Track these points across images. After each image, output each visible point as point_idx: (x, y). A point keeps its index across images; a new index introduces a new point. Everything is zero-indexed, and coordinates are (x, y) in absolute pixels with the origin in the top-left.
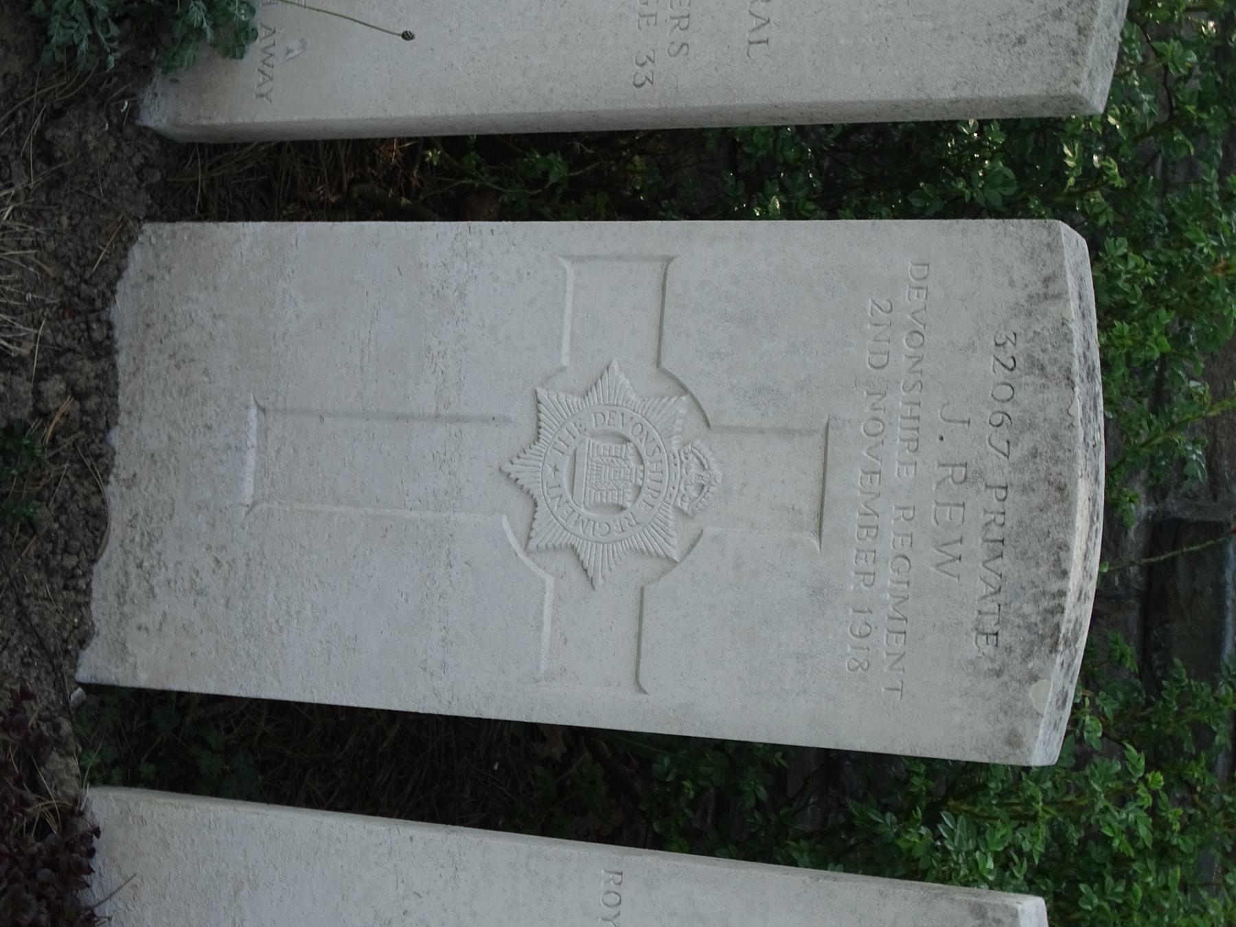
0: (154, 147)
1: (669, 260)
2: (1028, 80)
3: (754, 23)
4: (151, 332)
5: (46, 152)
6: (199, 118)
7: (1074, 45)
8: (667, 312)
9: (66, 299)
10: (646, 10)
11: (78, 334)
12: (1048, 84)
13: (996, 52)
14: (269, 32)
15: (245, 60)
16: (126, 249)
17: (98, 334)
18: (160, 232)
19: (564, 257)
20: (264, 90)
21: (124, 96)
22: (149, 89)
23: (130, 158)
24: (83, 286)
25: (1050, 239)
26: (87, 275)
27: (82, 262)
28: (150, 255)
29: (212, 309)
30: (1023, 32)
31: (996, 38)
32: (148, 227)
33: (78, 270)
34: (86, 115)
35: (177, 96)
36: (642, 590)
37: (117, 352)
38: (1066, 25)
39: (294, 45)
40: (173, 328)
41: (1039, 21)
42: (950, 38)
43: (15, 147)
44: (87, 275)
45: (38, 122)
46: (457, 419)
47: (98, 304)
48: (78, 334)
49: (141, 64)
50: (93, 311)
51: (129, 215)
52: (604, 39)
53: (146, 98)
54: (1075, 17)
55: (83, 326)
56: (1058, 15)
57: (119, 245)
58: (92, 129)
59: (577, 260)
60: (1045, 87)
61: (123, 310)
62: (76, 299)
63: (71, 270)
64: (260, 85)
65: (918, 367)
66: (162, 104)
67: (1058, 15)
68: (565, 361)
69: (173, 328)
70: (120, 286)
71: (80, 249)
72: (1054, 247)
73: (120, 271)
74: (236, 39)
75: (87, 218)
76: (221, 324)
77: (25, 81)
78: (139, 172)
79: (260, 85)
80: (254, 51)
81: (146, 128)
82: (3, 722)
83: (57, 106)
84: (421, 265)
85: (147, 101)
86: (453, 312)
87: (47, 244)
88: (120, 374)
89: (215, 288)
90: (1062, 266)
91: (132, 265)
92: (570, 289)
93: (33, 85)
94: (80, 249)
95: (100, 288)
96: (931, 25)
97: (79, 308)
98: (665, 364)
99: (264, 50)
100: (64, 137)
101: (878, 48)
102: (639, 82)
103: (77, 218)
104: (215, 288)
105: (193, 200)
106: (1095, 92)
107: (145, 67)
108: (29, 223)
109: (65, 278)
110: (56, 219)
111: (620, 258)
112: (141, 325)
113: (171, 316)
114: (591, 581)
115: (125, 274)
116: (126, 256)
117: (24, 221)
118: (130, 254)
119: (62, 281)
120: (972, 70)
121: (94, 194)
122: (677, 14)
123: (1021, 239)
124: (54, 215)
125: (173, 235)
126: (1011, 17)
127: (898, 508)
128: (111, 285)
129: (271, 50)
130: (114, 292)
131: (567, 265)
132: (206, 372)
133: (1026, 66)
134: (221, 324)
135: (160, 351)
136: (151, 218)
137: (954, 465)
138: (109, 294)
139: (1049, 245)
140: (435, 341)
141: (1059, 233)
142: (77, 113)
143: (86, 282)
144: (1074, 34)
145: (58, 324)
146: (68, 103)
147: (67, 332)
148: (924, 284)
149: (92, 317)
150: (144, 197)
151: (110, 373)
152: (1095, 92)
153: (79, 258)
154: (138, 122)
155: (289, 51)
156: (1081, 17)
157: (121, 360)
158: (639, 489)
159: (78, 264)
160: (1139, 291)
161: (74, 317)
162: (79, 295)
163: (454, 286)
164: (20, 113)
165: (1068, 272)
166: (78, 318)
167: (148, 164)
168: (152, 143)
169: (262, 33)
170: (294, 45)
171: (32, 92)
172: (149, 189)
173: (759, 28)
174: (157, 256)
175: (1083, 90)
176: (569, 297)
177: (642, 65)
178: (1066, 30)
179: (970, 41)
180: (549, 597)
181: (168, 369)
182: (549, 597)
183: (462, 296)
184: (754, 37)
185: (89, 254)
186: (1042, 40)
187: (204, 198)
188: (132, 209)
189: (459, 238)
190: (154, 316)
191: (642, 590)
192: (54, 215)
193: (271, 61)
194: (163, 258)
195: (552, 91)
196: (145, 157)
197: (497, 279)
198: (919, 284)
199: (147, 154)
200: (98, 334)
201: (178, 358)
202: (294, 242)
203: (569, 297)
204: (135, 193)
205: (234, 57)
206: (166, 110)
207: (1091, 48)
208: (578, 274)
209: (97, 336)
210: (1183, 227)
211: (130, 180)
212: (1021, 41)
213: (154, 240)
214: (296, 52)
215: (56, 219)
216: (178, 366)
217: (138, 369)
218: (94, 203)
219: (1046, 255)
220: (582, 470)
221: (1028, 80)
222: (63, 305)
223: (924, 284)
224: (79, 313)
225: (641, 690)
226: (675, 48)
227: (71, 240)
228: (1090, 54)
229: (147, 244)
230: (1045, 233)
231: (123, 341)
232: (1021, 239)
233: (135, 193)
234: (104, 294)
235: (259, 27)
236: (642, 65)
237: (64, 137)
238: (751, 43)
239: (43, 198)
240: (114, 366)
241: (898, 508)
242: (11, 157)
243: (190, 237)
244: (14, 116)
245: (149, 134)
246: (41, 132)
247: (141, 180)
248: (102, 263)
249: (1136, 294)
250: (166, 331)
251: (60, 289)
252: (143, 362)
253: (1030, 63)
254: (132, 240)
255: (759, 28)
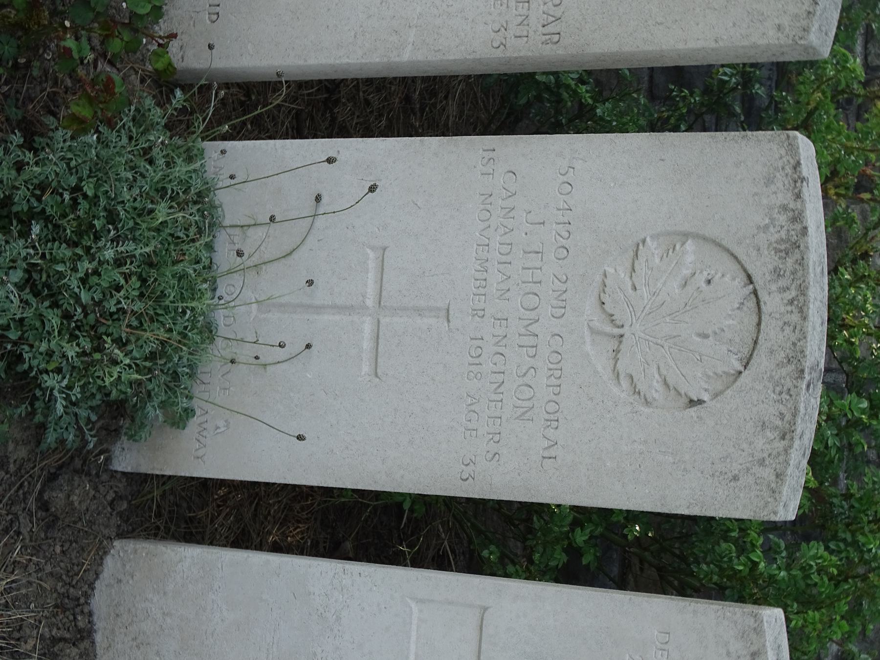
0: (121, 486)
1: (485, 609)
2: (741, 508)
3: (546, 444)
4: (119, 620)
5: (44, 506)
6: (153, 469)
7: (773, 485)
8: (484, 646)
9: (59, 601)
10: (470, 426)
11: (67, 625)
12: (755, 512)
13: (717, 484)
14: (203, 412)
15: (186, 431)
16: (102, 559)
17: (81, 622)
18: (126, 548)
19: (411, 599)
20: (200, 453)
21: (100, 453)
22: (118, 444)
23: (105, 496)
24: (72, 590)
25: (756, 625)
26: (74, 582)
27: (70, 574)
28: (119, 565)
29: (162, 608)
30: (736, 472)
31: (717, 474)
32: (117, 543)
33: (68, 580)
34: (73, 480)
35: (139, 452)
37: (95, 631)
38: (768, 470)
39: (221, 423)
40: (135, 619)
41: (748, 465)
42: (685, 470)
43: (23, 505)
44: (74, 582)
45: (39, 486)
47: (82, 600)
48: (67, 625)
49: (113, 428)
50: (79, 605)
51: (104, 536)
52: (440, 443)
53: (116, 450)
54: (774, 465)
55: (71, 618)
56: (762, 462)
57: (97, 557)
58: (77, 491)
60: (752, 514)
61: (101, 601)
62: (66, 601)
63: (63, 580)
64: (197, 450)
66: (128, 456)
67: (762, 462)
69: (135, 619)
70: (97, 584)
71: (69, 565)
72: (793, 149)
73: (97, 575)
74: (180, 419)
75: (74, 544)
76: (169, 620)
77: (29, 460)
78: (111, 503)
79: (197, 450)
80: (193, 424)
81: (116, 472)
82: (38, 2)
83: (53, 471)
84: (310, 593)
85: (117, 453)
86: (332, 630)
87: (45, 567)
88: (98, 648)
89: (165, 593)
90: (764, 646)
91: (106, 570)
92: (415, 622)
93: (36, 460)
94: (69, 565)
95: (83, 589)
96: (671, 459)
97: (69, 606)
99: (200, 424)
100: (57, 497)
101: (634, 472)
102: (465, 477)
103: (67, 545)
104: (165, 593)
105: (150, 508)
106: (821, 40)
107: (115, 430)
108: (32, 556)
109: (58, 588)
110: (52, 549)
111: (451, 603)
112: (112, 614)
113: (133, 610)
115: (101, 576)
116: (101, 564)
117: (28, 554)
118: (104, 562)
119: (56, 590)
120: (701, 495)
121: (79, 525)
122: (492, 431)
123: (736, 622)
124: (50, 545)
125: (135, 551)
126: (728, 460)
128: (91, 586)
129: (205, 426)
130: (93, 589)
131: (413, 605)
132: (158, 653)
133: (739, 497)
134: (169, 620)
135: (126, 635)
136: (121, 536)
138: (90, 592)
139: (755, 629)
140: (319, 650)
141: (762, 621)
142: (66, 477)
143: (73, 587)
144: (773, 478)
145: (53, 619)
146: (60, 467)
147: (60, 625)
148: (666, 647)
149: (78, 610)
150: (115, 520)
151: (90, 649)
152: (821, 40)
153: (68, 571)
154: (111, 468)
155: (218, 428)
156: (778, 466)
157: (98, 637)
159: (67, 575)
160: (826, 579)
161: (65, 612)
162: (68, 597)
163: (333, 611)
164: (26, 483)
165: (769, 649)
166: (67, 613)
167: (119, 497)
168: (120, 481)
169: (198, 412)
170: (221, 423)
171: (35, 466)
172: (120, 514)
173: (550, 447)
174: (124, 565)
175: (814, 38)
176: (414, 627)
177: (467, 465)
178: (768, 474)
179: (699, 475)
181: (131, 648)
183: (338, 619)
184: (546, 454)
185: (76, 568)
186: (751, 480)
187: (158, 506)
188: (106, 532)
189: (336, 576)
190: (122, 608)
192: (50, 545)
193: (205, 433)
194: (128, 567)
195: (402, 477)
196: (115, 492)
197: (363, 609)
198: (663, 646)
199: (117, 490)
200: (81, 622)
201: (138, 641)
202: (220, 566)
203: (414, 627)
204: (109, 519)
205: (178, 427)
206: (128, 459)
207: (785, 489)
208: (421, 611)
209: (81, 624)
211: (105, 511)
212: (735, 478)
213: (121, 554)
214: (223, 429)
215: (52, 549)
216: (138, 647)
217: (110, 646)
218: (79, 532)
219: (753, 636)
221: (741, 508)
222: (56, 606)
223: (666, 647)
224: (69, 610)
226: (490, 456)
227: (62, 561)
228: (785, 493)
229: (117, 556)
230: (753, 620)
231: (100, 624)
232: (736, 622)
233: (109, 519)
234: (86, 592)
235: (196, 408)
236: (467, 465)
237: (57, 497)
238: (544, 458)
239: (43, 535)
240: (93, 643)
242: (20, 513)
243: (147, 554)
244: (21, 486)
245: (119, 476)
246: (41, 493)
247: (113, 509)
248: (85, 571)
249: (824, 582)
250: (130, 620)
251: (55, 595)
252: (114, 641)
253: (741, 495)
254: (106, 553)
255: (550, 447)
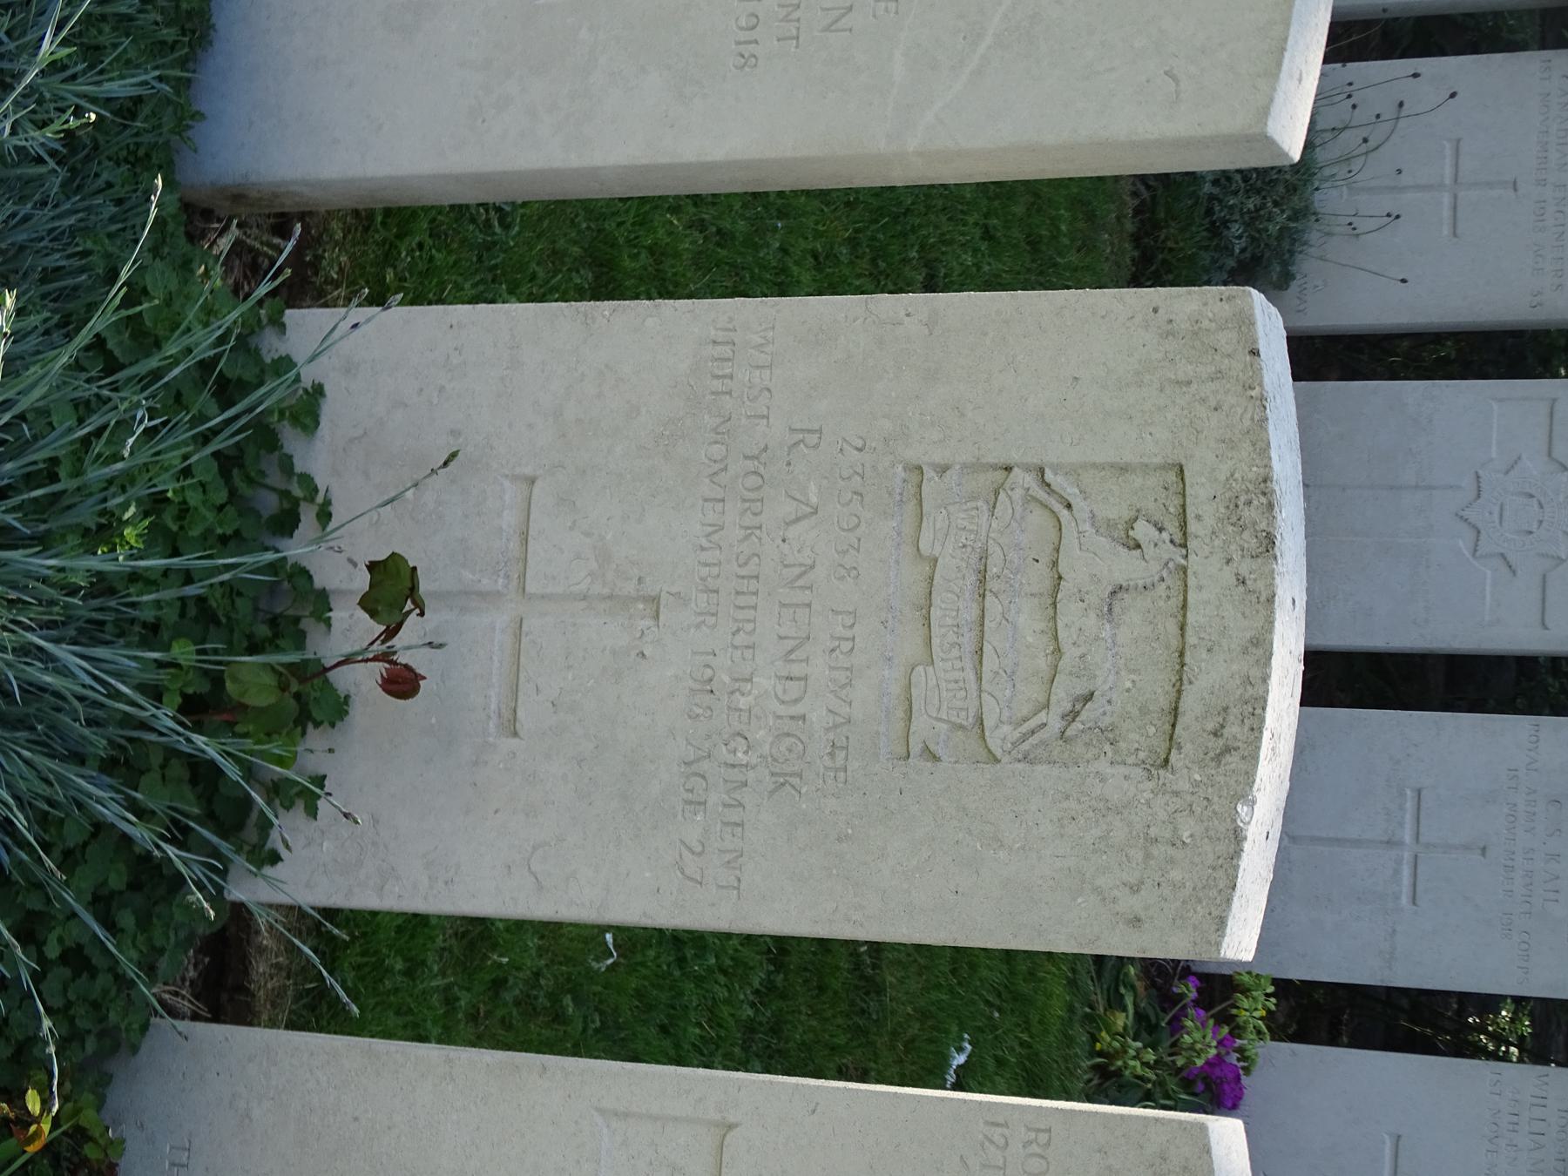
1: (1554, 400)
36: (1544, 576)
46: (1430, 488)
59: (1501, 400)
65: (795, 15)
68: (1494, 455)
98: (1555, 454)
114: (1514, 573)
127: (987, 1123)
137: (1038, 1130)
158: (1541, 522)
180: (1489, 581)
182: (1489, 581)
191: (1544, 576)
210: (1234, 1011)
220: (1507, 514)
225: (1544, 626)
241: (987, 1123)
